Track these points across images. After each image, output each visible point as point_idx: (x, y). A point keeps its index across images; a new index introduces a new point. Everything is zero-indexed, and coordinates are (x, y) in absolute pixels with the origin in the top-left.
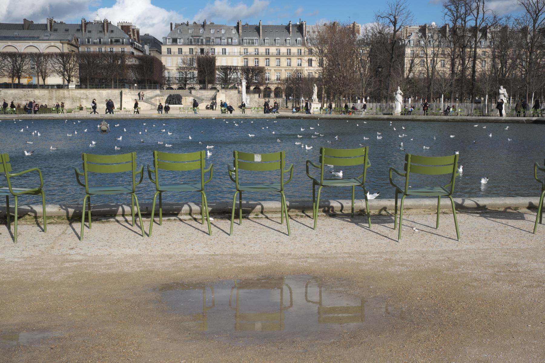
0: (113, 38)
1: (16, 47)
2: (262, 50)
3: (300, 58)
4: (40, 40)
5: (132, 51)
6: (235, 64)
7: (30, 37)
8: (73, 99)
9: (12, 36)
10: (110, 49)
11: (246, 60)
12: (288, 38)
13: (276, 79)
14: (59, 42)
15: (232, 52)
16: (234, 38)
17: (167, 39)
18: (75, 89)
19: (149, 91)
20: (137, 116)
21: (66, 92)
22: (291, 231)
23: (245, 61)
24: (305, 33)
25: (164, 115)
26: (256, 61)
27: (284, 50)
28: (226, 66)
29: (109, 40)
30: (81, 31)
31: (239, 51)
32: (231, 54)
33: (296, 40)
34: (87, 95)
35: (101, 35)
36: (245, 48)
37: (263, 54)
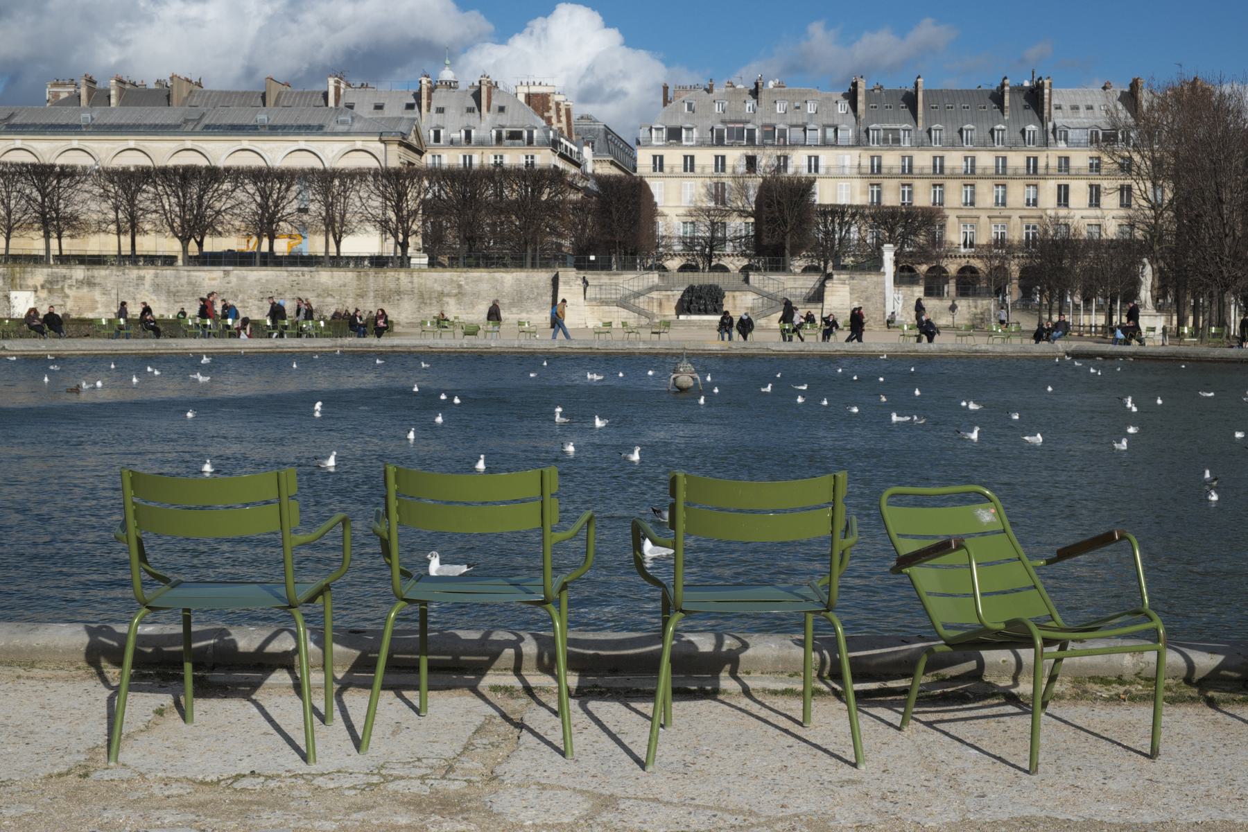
0: (503, 127)
1: (263, 154)
2: (923, 160)
3: (1034, 182)
4: (325, 134)
5: (553, 162)
6: (843, 200)
7: (299, 127)
8: (421, 296)
9: (253, 123)
10: (496, 157)
11: (875, 189)
12: (998, 127)
13: (962, 242)
14: (377, 138)
15: (838, 167)
16: (844, 126)
17: (653, 130)
18: (426, 267)
19: (630, 276)
20: (557, 343)
21: (403, 275)
22: (1164, 719)
23: (873, 192)
24: (1050, 110)
25: (739, 346)
26: (904, 192)
27: (986, 160)
28: (831, 205)
29: (494, 133)
30: (416, 108)
31: (857, 163)
32: (833, 171)
33: (1023, 132)
34: (460, 286)
35: (472, 119)
36: (873, 153)
37: (926, 171)
